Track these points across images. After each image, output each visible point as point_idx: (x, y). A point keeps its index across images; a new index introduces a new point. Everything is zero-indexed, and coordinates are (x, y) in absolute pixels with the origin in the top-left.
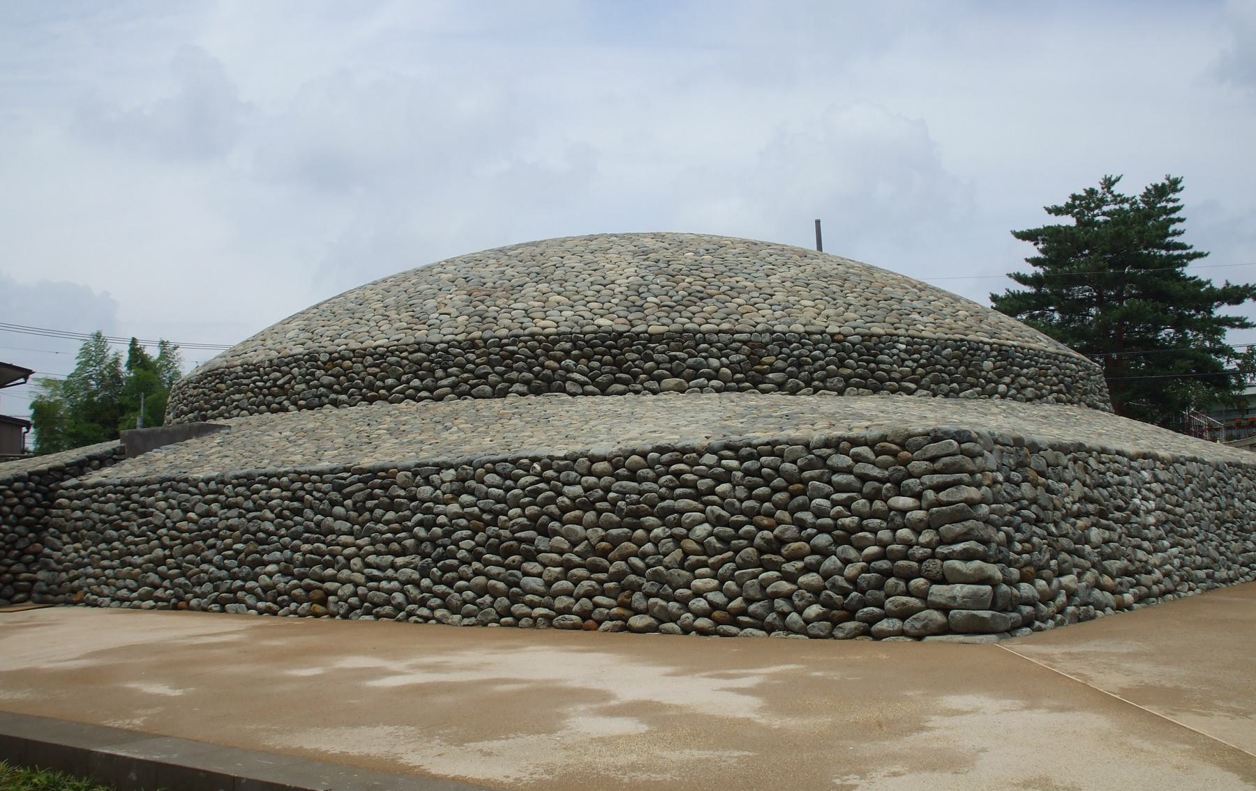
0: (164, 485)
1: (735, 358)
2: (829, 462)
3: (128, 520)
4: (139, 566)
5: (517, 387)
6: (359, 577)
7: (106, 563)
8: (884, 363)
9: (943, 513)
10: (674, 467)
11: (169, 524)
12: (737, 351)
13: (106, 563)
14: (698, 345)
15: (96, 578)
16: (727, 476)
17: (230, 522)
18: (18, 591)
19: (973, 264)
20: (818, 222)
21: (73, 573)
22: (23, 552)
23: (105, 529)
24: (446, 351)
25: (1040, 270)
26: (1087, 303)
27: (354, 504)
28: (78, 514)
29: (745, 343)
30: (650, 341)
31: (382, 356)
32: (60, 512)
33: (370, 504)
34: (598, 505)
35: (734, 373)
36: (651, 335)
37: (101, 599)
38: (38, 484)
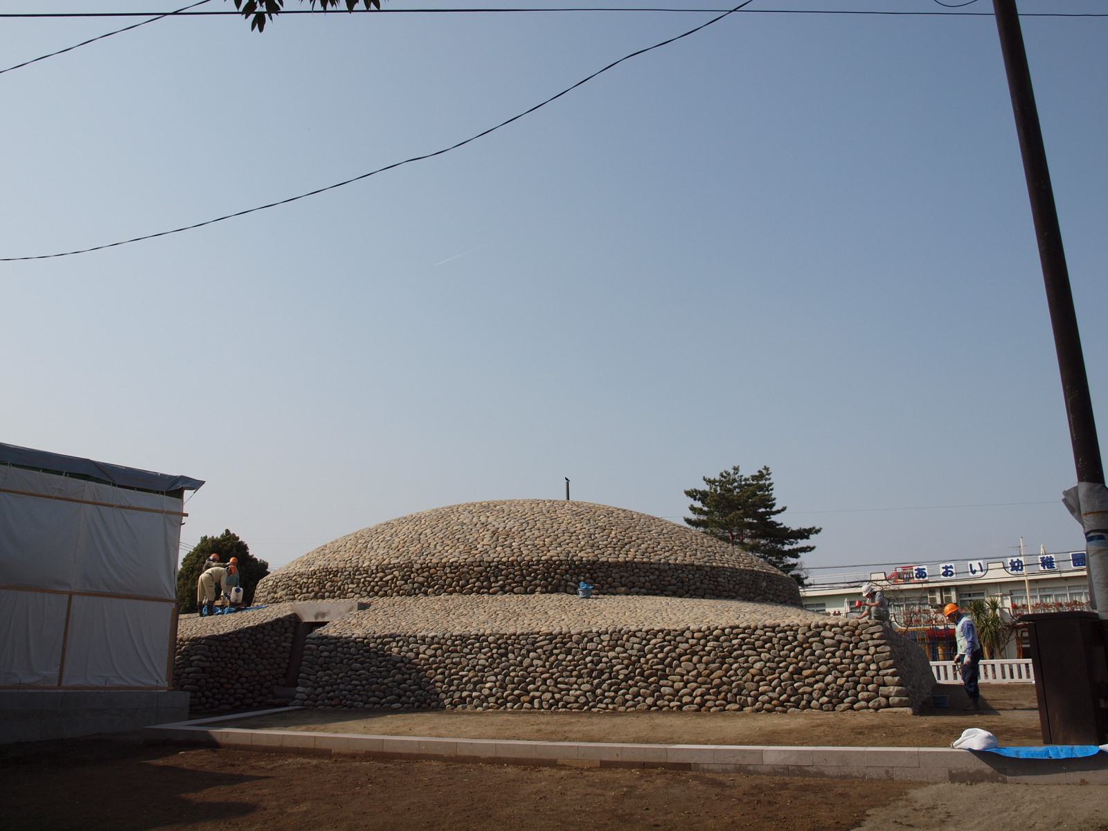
1: (652, 577)
5: (539, 589)
8: (721, 582)
9: (882, 657)
15: (350, 691)
17: (454, 660)
21: (328, 688)
22: (240, 676)
23: (352, 663)
24: (497, 567)
25: (703, 517)
28: (326, 654)
29: (656, 569)
31: (456, 568)
33: (555, 651)
35: (651, 585)
37: (356, 704)
38: (251, 634)
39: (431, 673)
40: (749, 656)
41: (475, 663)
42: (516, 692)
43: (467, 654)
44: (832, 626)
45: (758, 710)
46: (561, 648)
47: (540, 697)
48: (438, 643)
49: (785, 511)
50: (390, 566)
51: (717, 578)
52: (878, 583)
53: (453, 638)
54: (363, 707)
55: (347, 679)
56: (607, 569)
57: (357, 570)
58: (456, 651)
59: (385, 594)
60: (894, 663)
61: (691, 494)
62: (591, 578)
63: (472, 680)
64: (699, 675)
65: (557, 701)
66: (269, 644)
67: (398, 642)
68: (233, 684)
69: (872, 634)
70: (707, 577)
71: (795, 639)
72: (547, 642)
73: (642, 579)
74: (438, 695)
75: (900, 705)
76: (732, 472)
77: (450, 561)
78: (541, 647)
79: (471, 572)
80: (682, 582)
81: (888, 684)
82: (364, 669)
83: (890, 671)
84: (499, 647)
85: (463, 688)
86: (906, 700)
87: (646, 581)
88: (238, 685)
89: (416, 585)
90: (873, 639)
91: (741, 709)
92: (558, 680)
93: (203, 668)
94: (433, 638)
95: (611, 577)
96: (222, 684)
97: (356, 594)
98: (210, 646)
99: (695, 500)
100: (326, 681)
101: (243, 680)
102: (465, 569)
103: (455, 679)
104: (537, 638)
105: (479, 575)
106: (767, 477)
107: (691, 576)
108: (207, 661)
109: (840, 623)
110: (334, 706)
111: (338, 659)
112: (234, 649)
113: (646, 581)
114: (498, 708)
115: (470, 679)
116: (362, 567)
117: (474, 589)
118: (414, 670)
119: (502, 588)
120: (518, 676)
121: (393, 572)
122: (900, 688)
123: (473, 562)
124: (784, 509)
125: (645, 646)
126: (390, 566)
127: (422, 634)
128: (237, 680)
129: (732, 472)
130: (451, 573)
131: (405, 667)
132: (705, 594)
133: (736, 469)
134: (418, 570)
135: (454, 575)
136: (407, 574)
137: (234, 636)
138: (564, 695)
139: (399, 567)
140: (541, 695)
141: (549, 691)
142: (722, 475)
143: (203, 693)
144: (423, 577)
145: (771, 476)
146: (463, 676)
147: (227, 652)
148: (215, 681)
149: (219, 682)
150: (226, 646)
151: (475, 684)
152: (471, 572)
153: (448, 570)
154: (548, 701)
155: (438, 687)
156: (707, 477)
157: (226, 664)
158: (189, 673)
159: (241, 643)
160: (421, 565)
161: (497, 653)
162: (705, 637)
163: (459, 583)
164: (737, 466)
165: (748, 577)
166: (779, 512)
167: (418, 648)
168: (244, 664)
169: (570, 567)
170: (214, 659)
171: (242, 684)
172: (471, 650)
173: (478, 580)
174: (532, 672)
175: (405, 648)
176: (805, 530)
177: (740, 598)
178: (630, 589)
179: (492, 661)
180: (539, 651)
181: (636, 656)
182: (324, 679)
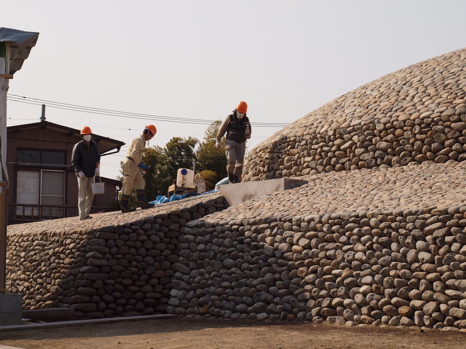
0: (272, 224)
3: (242, 251)
4: (255, 286)
6: (442, 298)
7: (225, 284)
11: (278, 254)
13: (225, 284)
15: (219, 295)
17: (328, 253)
18: (147, 305)
20: (44, 106)
21: (199, 291)
22: (150, 277)
23: (225, 258)
27: (435, 239)
28: (201, 246)
31: (428, 125)
32: (186, 245)
33: (448, 239)
37: (223, 312)
38: (162, 225)
39: (302, 272)
41: (350, 257)
42: (394, 300)
43: (345, 244)
46: (456, 233)
47: (421, 308)
48: (315, 229)
50: (348, 129)
53: (330, 221)
54: (229, 317)
55: (218, 279)
57: (315, 137)
58: (333, 240)
59: (343, 168)
63: (345, 281)
65: (445, 314)
66: (138, 235)
67: (272, 228)
68: (141, 287)
72: (439, 224)
74: (306, 301)
77: (421, 116)
78: (431, 232)
79: (447, 130)
82: (235, 266)
84: (380, 235)
85: (334, 292)
88: (148, 288)
89: (378, 153)
92: (447, 283)
93: (100, 267)
94: (309, 221)
96: (126, 287)
97: (312, 169)
98: (107, 240)
100: (198, 282)
101: (154, 281)
102: (439, 127)
103: (326, 280)
104: (426, 219)
105: (458, 134)
108: (104, 258)
110: (202, 314)
111: (212, 253)
112: (139, 244)
114: (370, 323)
115: (343, 279)
116: (319, 133)
117: (450, 155)
118: (285, 268)
120: (399, 277)
121: (352, 136)
123: (450, 116)
126: (348, 129)
127: (298, 217)
128: (147, 282)
130: (421, 133)
131: (276, 263)
134: (380, 132)
135: (424, 136)
136: (367, 138)
137: (138, 227)
138: (453, 306)
139: (357, 130)
140: (423, 305)
141: (434, 300)
143: (101, 296)
144: (386, 141)
146: (337, 276)
147: (129, 247)
148: (116, 283)
149: (121, 284)
150: (129, 240)
151: (349, 286)
152: (447, 130)
153: (417, 129)
154: (430, 315)
155: (307, 291)
157: (130, 262)
158: (83, 273)
160: (385, 124)
161: (377, 242)
163: (431, 146)
167: (292, 236)
168: (156, 261)
170: (113, 255)
171: (153, 286)
172: (349, 238)
173: (456, 140)
174: (415, 270)
175: (278, 237)
179: (370, 254)
180: (428, 238)
182: (196, 280)
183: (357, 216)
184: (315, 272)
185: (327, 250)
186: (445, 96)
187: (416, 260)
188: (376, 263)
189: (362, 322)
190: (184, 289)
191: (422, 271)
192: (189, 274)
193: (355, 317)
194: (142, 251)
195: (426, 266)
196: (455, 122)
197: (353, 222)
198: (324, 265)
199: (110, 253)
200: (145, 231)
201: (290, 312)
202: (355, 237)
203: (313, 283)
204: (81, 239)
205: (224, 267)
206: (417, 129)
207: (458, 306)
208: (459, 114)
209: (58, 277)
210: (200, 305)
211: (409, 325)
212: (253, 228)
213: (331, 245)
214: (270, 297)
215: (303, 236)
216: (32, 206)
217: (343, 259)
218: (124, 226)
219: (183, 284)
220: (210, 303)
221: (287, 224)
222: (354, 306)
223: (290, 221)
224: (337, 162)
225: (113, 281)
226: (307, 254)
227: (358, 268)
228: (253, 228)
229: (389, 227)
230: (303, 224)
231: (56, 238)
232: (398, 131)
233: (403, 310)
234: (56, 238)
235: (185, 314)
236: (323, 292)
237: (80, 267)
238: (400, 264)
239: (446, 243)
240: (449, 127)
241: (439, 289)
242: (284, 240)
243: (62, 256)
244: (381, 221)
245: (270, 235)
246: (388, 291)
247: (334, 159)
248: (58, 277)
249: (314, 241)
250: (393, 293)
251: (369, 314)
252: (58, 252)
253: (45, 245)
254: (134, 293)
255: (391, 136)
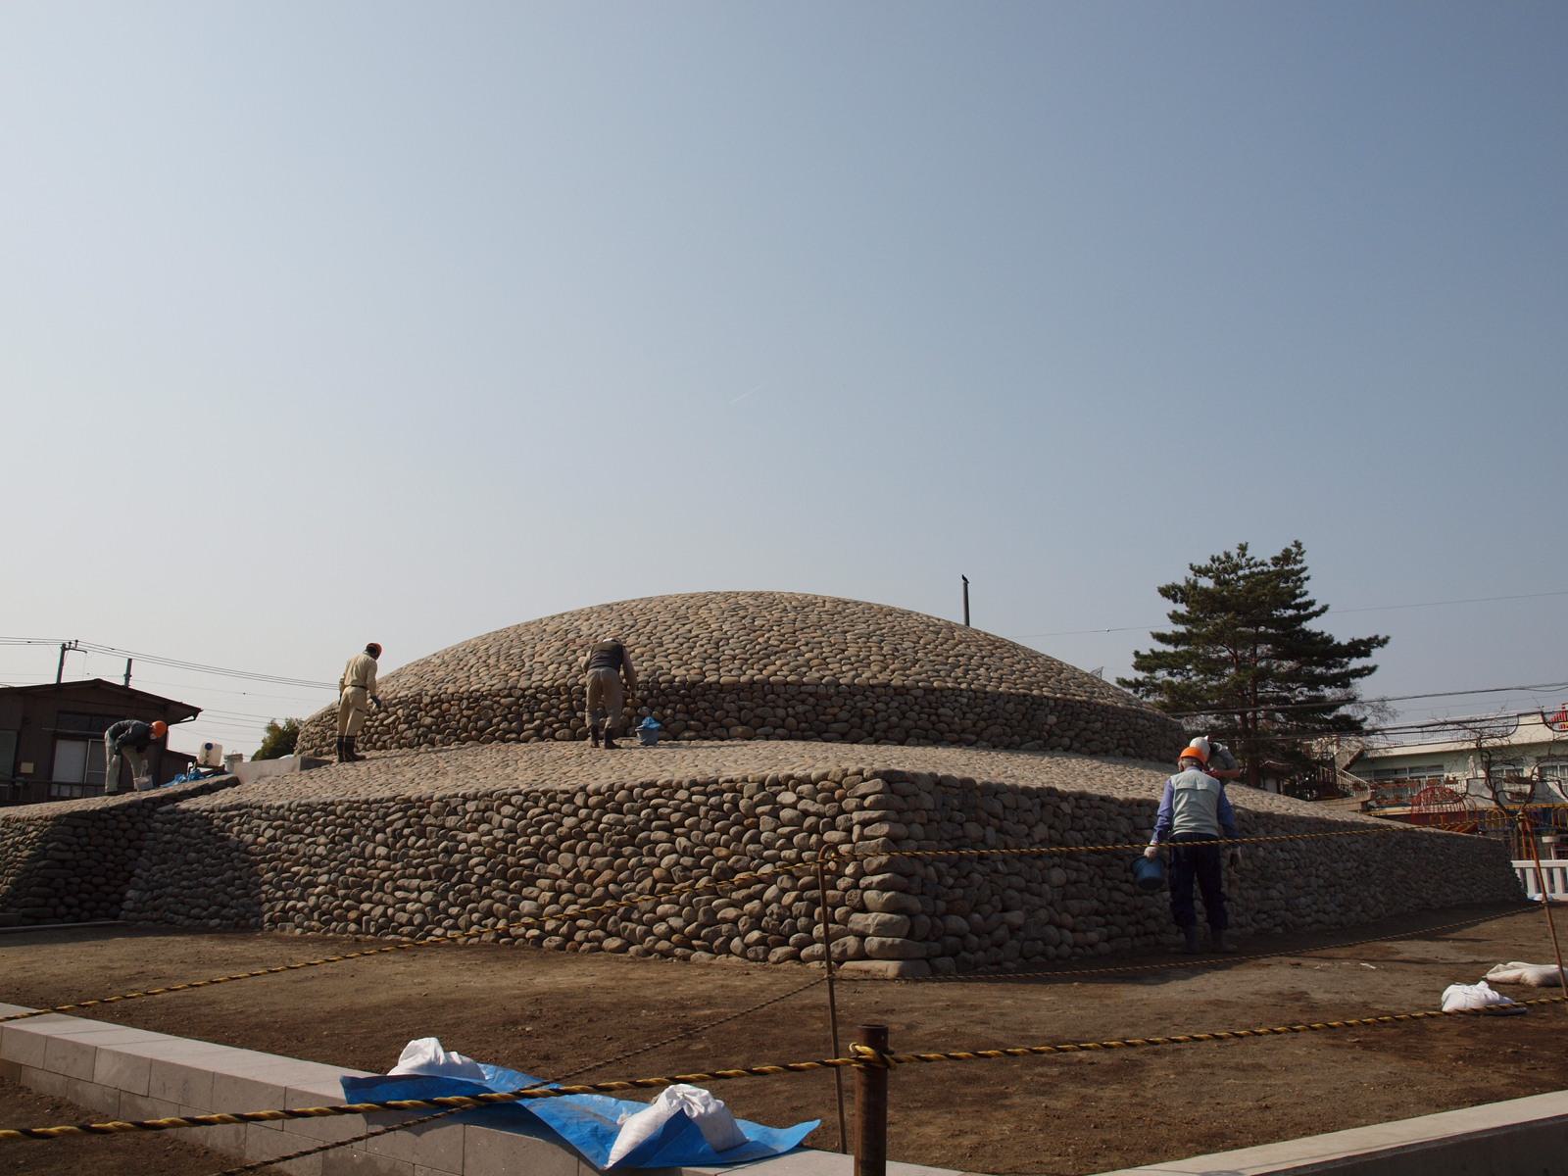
1: (800, 708)
2: (778, 799)
4: (213, 886)
6: (391, 901)
7: (184, 883)
10: (653, 802)
12: (803, 702)
13: (184, 883)
14: (766, 695)
15: (176, 896)
16: (693, 811)
19: (1101, 626)
20: (130, 660)
21: (156, 892)
24: (533, 696)
25: (1181, 629)
26: (1225, 663)
29: (811, 694)
30: (721, 691)
31: (477, 700)
33: (406, 831)
34: (589, 835)
35: (799, 723)
36: (722, 685)
39: (262, 869)
40: (657, 842)
43: (309, 836)
44: (801, 781)
45: (648, 952)
46: (416, 823)
49: (1327, 613)
51: (937, 709)
52: (1471, 725)
56: (716, 697)
59: (384, 747)
60: (890, 861)
61: (1168, 592)
62: (687, 712)
64: (578, 877)
67: (242, 816)
69: (864, 797)
70: (917, 708)
71: (735, 806)
72: (400, 814)
73: (781, 712)
74: (261, 904)
75: (883, 954)
76: (1234, 553)
78: (392, 823)
80: (863, 717)
81: (870, 906)
82: (198, 862)
83: (877, 878)
84: (345, 826)
86: (892, 945)
87: (788, 715)
90: (864, 809)
91: (623, 949)
93: (63, 861)
95: (722, 709)
96: (97, 887)
99: (1176, 601)
103: (285, 879)
104: (389, 808)
106: (1298, 558)
107: (880, 706)
109: (813, 776)
110: (155, 921)
111: (177, 845)
113: (788, 715)
114: (319, 930)
119: (538, 731)
122: (888, 916)
124: (1324, 609)
125: (519, 820)
129: (1234, 553)
130: (468, 708)
132: (908, 737)
133: (1243, 548)
134: (427, 705)
139: (402, 702)
140: (372, 909)
141: (384, 904)
142: (1213, 560)
144: (432, 717)
145: (1305, 556)
146: (296, 874)
147: (106, 837)
148: (83, 881)
149: (91, 883)
152: (496, 706)
155: (263, 892)
156: (1196, 564)
157: (105, 855)
158: (40, 869)
159: (133, 824)
162: (601, 805)
164: (1244, 543)
165: (1010, 707)
166: (1317, 614)
167: (259, 826)
169: (651, 693)
173: (505, 718)
176: (1361, 642)
177: (984, 744)
178: (755, 730)
181: (502, 839)
183: (325, 803)
184: (274, 869)
185: (291, 843)
186: (502, 667)
187: (373, 856)
188: (335, 859)
189: (311, 929)
190: (141, 889)
191: (377, 869)
192: (149, 871)
193: (306, 923)
194: (123, 842)
195: (381, 863)
196: (505, 697)
197: (320, 810)
198: (285, 861)
199: (78, 844)
200: (129, 817)
201: (243, 917)
202: (319, 828)
203: (270, 883)
204: (46, 826)
205: (187, 863)
206: (465, 702)
207: (405, 911)
208: (510, 689)
209: (12, 875)
210: (156, 909)
211: (356, 932)
212: (223, 815)
213: (296, 838)
214: (226, 899)
215: (269, 826)
216: (71, 785)
217: (304, 855)
218: (100, 811)
219: (142, 884)
220: (165, 907)
221: (257, 811)
222: (306, 910)
223: (260, 807)
224: (378, 740)
225: (79, 880)
226: (270, 847)
227: (317, 865)
228: (223, 815)
229: (354, 817)
230: (272, 812)
231: (18, 825)
232: (445, 706)
233: (353, 915)
234: (18, 825)
235: (137, 921)
236: (280, 893)
237: (38, 861)
238: (357, 860)
239: (404, 837)
240: (498, 702)
241: (389, 890)
242: (250, 831)
243: (21, 847)
244: (347, 810)
245: (238, 824)
246: (341, 892)
247: (376, 736)
248: (12, 875)
249: (279, 832)
250: (345, 894)
251: (319, 920)
252: (17, 842)
253: (5, 833)
254: (108, 894)
255: (437, 711)
